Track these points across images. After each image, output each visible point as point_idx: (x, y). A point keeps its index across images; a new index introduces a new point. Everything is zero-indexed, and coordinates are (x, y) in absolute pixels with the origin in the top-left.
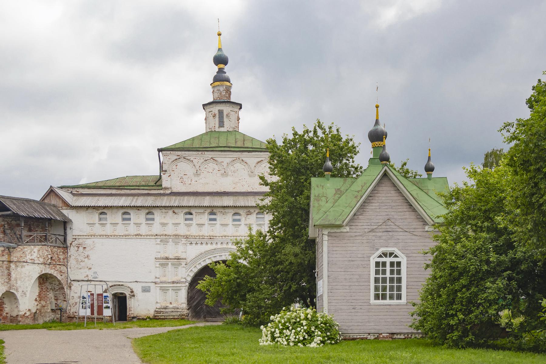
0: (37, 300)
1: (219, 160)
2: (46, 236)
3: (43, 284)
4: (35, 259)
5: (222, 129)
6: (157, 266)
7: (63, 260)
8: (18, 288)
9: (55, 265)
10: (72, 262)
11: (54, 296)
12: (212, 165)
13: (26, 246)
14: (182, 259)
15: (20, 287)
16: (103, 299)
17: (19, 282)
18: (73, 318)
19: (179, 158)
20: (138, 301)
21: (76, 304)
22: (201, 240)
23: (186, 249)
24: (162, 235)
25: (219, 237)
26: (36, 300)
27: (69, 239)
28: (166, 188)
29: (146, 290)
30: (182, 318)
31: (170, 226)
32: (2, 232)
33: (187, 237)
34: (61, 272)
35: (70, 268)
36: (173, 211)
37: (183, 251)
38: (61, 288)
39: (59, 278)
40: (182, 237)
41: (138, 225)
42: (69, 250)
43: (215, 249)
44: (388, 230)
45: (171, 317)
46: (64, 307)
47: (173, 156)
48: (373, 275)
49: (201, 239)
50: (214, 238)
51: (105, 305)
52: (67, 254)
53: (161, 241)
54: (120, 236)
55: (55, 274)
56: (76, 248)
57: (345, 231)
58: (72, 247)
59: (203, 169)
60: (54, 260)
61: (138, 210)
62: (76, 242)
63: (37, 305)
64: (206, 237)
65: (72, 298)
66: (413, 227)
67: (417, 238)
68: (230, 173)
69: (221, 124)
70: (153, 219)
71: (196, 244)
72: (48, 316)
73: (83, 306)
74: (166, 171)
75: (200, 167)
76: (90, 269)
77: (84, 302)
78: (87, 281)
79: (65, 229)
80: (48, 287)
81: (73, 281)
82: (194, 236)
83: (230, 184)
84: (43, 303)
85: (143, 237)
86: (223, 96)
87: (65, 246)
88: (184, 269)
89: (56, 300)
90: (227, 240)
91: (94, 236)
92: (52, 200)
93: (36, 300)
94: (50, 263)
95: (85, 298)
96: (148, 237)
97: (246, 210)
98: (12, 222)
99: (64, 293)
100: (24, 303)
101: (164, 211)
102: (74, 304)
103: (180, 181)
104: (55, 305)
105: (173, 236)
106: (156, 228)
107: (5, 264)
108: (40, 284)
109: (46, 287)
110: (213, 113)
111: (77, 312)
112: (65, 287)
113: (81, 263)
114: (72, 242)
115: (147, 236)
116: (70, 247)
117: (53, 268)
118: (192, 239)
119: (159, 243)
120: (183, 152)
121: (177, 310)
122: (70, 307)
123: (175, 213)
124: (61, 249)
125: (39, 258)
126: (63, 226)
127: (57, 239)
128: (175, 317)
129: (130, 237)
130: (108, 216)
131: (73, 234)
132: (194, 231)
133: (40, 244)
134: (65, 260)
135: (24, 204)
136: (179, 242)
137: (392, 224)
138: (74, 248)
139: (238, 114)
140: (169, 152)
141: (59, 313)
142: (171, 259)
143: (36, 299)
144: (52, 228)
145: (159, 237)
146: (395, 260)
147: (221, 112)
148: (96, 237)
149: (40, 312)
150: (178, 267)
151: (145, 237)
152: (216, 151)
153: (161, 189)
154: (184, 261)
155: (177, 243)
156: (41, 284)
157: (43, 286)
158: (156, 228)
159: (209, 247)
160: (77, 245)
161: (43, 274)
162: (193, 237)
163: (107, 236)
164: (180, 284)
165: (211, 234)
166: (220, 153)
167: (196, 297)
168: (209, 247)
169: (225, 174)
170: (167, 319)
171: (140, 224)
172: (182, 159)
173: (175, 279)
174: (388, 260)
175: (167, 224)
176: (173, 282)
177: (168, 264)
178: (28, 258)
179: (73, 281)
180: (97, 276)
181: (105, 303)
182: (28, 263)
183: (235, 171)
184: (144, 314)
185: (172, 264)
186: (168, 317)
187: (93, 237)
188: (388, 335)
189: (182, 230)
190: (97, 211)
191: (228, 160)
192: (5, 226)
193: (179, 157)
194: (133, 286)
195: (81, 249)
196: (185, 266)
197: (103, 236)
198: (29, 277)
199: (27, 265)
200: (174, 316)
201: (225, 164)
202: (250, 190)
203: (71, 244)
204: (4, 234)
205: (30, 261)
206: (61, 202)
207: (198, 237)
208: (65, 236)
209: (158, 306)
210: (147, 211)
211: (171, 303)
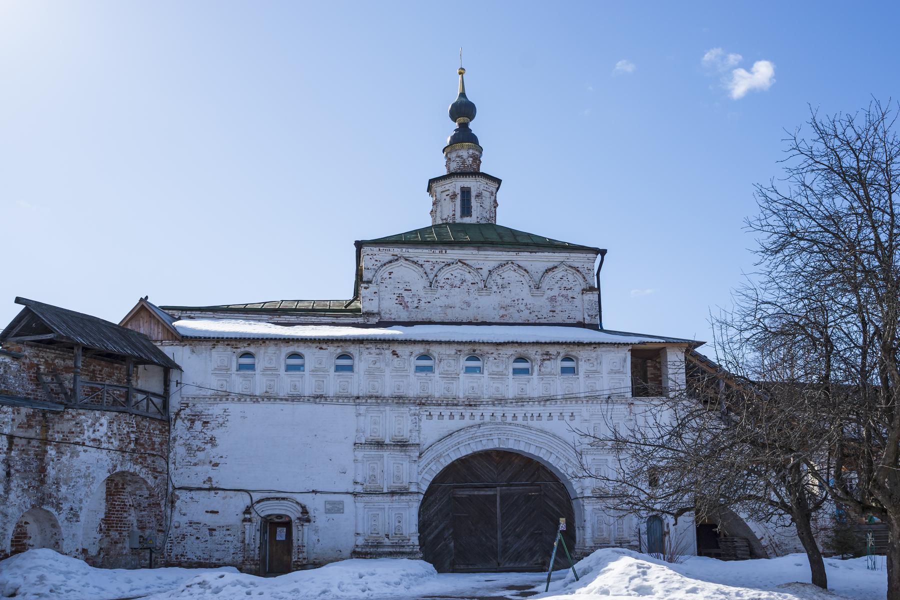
4: (102, 440)
7: (159, 446)
8: (61, 502)
10: (179, 451)
13: (81, 411)
15: (66, 499)
17: (64, 489)
21: (184, 538)
32: (31, 380)
35: (174, 463)
36: (394, 351)
38: (153, 504)
42: (172, 427)
46: (159, 543)
47: (385, 254)
52: (169, 433)
55: (143, 473)
58: (179, 422)
60: (142, 445)
61: (321, 348)
62: (188, 411)
69: (466, 210)
81: (179, 488)
86: (468, 166)
87: (164, 418)
92: (142, 325)
98: (56, 361)
100: (74, 535)
107: (34, 447)
109: (122, 502)
113: (198, 453)
114: (181, 410)
117: (140, 460)
122: (169, 545)
123: (397, 354)
125: (111, 438)
134: (164, 447)
138: (182, 423)
139: (496, 197)
156: (110, 495)
160: (191, 417)
162: (816, 128)
172: (402, 262)
179: (179, 488)
183: (504, 286)
192: (39, 369)
194: (308, 500)
195: (198, 425)
199: (85, 451)
204: (37, 385)
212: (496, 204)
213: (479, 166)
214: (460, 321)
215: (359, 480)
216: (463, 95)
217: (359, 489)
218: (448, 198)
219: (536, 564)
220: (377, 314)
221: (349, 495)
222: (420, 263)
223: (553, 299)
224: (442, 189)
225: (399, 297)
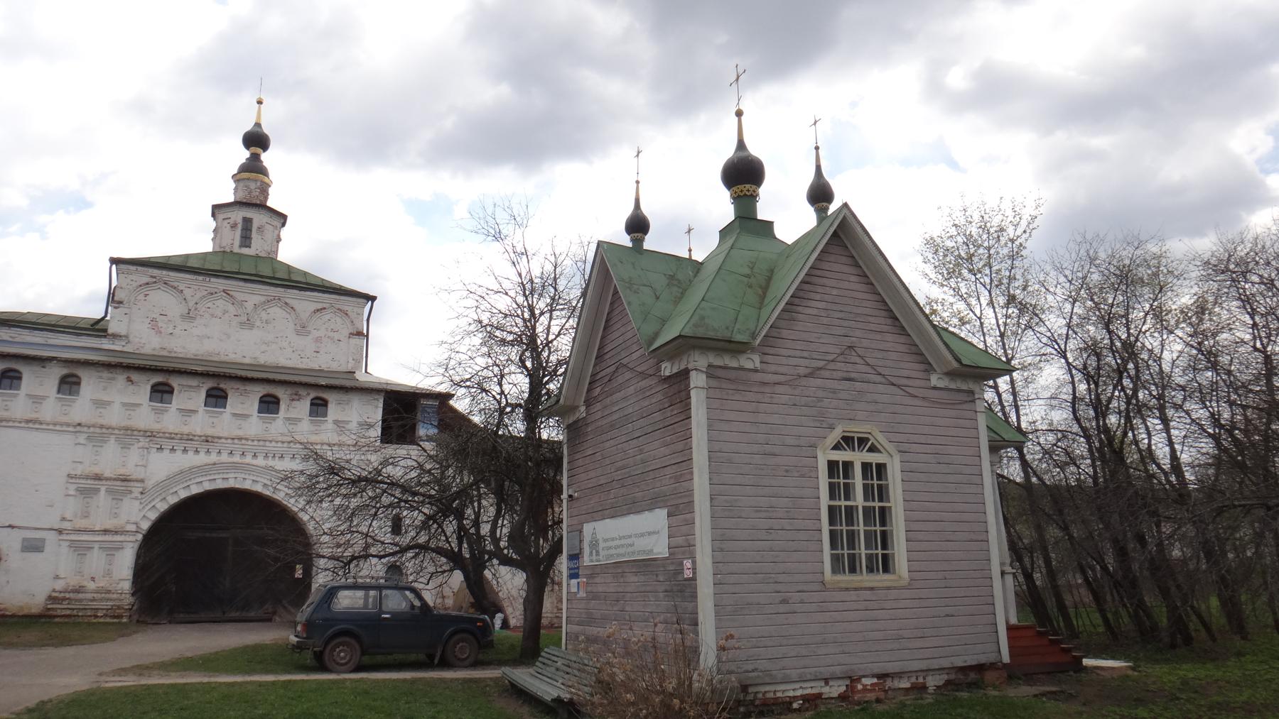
1: (239, 296)
5: (245, 251)
6: (72, 492)
12: (221, 304)
14: (137, 481)
19: (155, 282)
22: (187, 441)
23: (147, 460)
24: (94, 426)
25: (227, 439)
28: (116, 336)
29: (34, 546)
30: (114, 613)
36: (128, 377)
37: (138, 464)
43: (215, 464)
44: (853, 375)
47: (143, 276)
48: (825, 501)
49: (184, 441)
57: (749, 365)
59: (204, 309)
61: (43, 367)
66: (906, 373)
67: (916, 402)
68: (258, 323)
69: (246, 240)
71: (173, 450)
74: (121, 302)
75: (196, 303)
82: (171, 433)
83: (255, 344)
85: (44, 427)
88: (137, 503)
90: (244, 447)
96: (58, 428)
97: (290, 391)
101: (106, 374)
105: (120, 430)
110: (231, 221)
115: (55, 424)
120: (164, 272)
121: (107, 596)
123: (131, 381)
129: (11, 424)
136: (130, 444)
137: (858, 360)
139: (280, 232)
140: (139, 268)
145: (85, 429)
146: (874, 458)
147: (247, 222)
150: (121, 498)
151: (51, 427)
152: (237, 279)
154: (139, 485)
155: (126, 447)
159: (202, 459)
162: (167, 435)
164: (123, 536)
165: (210, 432)
166: (241, 284)
168: (202, 459)
169: (248, 324)
171: (44, 398)
173: (109, 524)
174: (858, 458)
175: (109, 403)
176: (106, 531)
177: (98, 490)
183: (268, 322)
188: (875, 680)
191: (257, 299)
193: (155, 280)
196: (140, 496)
201: (249, 305)
209: (59, 585)
210: (65, 371)
211: (93, 579)
212: (278, 240)
213: (266, 198)
214: (263, 362)
215: (68, 516)
216: (741, 145)
217: (66, 525)
218: (228, 226)
219: (265, 613)
220: (125, 336)
221: (54, 532)
222: (181, 288)
223: (318, 340)
224: (225, 216)
225: (152, 321)
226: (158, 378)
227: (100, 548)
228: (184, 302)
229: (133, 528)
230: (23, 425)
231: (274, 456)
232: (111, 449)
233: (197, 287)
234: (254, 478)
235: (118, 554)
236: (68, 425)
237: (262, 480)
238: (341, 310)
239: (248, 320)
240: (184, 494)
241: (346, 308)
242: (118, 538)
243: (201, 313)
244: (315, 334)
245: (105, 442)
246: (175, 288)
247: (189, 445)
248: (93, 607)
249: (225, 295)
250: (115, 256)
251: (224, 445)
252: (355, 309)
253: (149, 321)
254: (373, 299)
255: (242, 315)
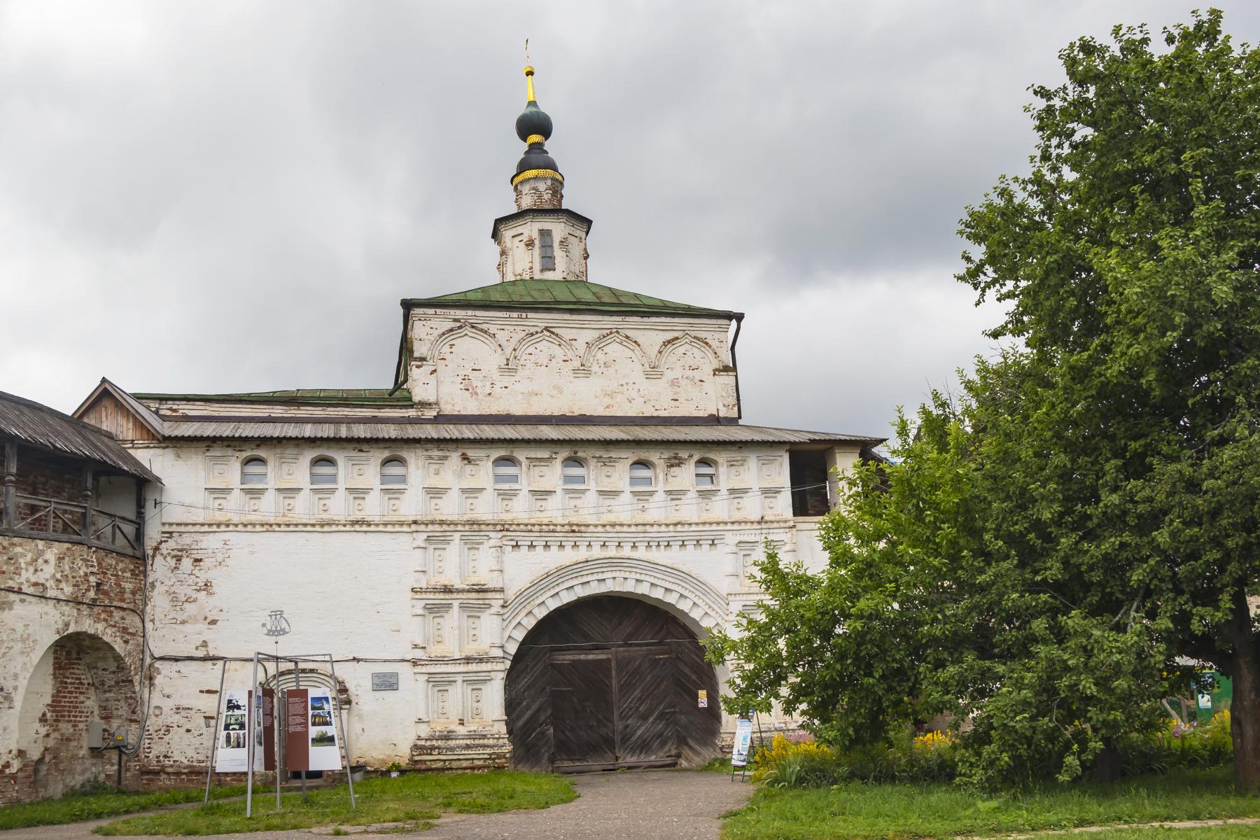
0: (46, 721)
1: (566, 334)
2: (84, 515)
3: (66, 669)
7: (131, 596)
9: (108, 609)
10: (158, 603)
11: (100, 706)
12: (545, 347)
14: (495, 591)
16: (306, 708)
18: (157, 773)
19: (460, 327)
20: (360, 717)
21: (168, 731)
22: (545, 534)
24: (433, 523)
25: (596, 526)
26: (43, 719)
27: (153, 534)
28: (424, 405)
29: (386, 683)
30: (496, 767)
31: (454, 497)
33: (504, 527)
34: (125, 630)
35: (153, 621)
36: (463, 454)
38: (123, 681)
39: (118, 649)
40: (491, 527)
41: (358, 493)
42: (149, 567)
45: (465, 764)
46: (132, 739)
49: (543, 534)
50: (583, 529)
51: (314, 732)
52: (145, 576)
53: (428, 539)
54: (305, 525)
55: (108, 635)
56: (172, 562)
58: (159, 559)
59: (524, 357)
60: (106, 593)
61: (361, 451)
62: (171, 544)
63: (47, 735)
64: (559, 528)
65: (157, 712)
68: (595, 368)
69: (548, 263)
70: (403, 479)
71: (532, 546)
72: (79, 768)
73: (228, 737)
75: (515, 350)
76: (214, 622)
77: (233, 721)
78: (205, 659)
79: (140, 505)
80: (83, 677)
81: (162, 658)
82: (526, 525)
83: (596, 397)
84: (66, 728)
85: (373, 528)
87: (138, 554)
89: (107, 718)
91: (228, 525)
92: (104, 419)
93: (43, 719)
94: (94, 600)
95: (238, 707)
96: (390, 528)
99: (131, 698)
101: (436, 453)
102: (162, 732)
103: (462, 386)
104: (101, 733)
106: (412, 504)
108: (58, 666)
109: (77, 679)
110: (525, 238)
111: (169, 754)
112: (137, 679)
113: (187, 605)
115: (385, 525)
116: (154, 556)
118: (519, 534)
119: (423, 545)
120: (470, 313)
121: (481, 742)
122: (147, 741)
123: (468, 459)
124: (127, 561)
126: (134, 496)
127: (117, 530)
128: (477, 763)
129: (334, 528)
130: (270, 469)
131: (164, 520)
132: (521, 509)
133: (65, 537)
134: (137, 597)
135: (22, 413)
140: (431, 311)
141: (114, 756)
142: (458, 591)
143: (44, 715)
144: (100, 501)
145: (422, 528)
147: (545, 234)
148: (231, 528)
149: (55, 758)
150: (477, 614)
153: (412, 406)
154: (498, 595)
156: (60, 668)
157: (67, 675)
158: (412, 504)
159: (569, 556)
160: (175, 553)
161: (69, 636)
163: (268, 526)
164: (489, 664)
167: (524, 703)
169: (583, 370)
170: (452, 769)
171: (366, 491)
173: (471, 650)
176: (468, 660)
177: (449, 606)
178: (26, 576)
179: (162, 658)
180: (284, 625)
181: (314, 724)
182: (23, 597)
184: (381, 757)
185: (463, 607)
186: (455, 764)
187: (223, 528)
189: (486, 507)
190: (238, 454)
191: (590, 335)
193: (459, 324)
195: (187, 563)
197: (254, 525)
198: (23, 640)
199: (22, 601)
200: (473, 759)
201: (581, 346)
202: (649, 412)
203: (156, 549)
205: (31, 590)
206: (131, 425)
207: (537, 528)
208: (139, 524)
209: (424, 731)
211: (462, 722)
217: (419, 654)
218: (522, 245)
223: (674, 383)
224: (514, 232)
226: (502, 452)
227: (464, 681)
228: (499, 349)
229: (499, 653)
230: (348, 528)
231: (659, 545)
232: (455, 549)
233: (512, 328)
234: (638, 577)
235: (487, 688)
236: (401, 524)
237: (647, 578)
238: (698, 339)
239: (582, 365)
240: (553, 605)
241: (702, 335)
242: (484, 667)
243: (522, 362)
244: (670, 375)
245: (448, 542)
246: (486, 332)
247: (551, 539)
248: (468, 757)
249: (548, 334)
250: (409, 296)
251: (594, 535)
252: (717, 335)
253: (459, 380)
254: (739, 317)
255: (574, 359)
